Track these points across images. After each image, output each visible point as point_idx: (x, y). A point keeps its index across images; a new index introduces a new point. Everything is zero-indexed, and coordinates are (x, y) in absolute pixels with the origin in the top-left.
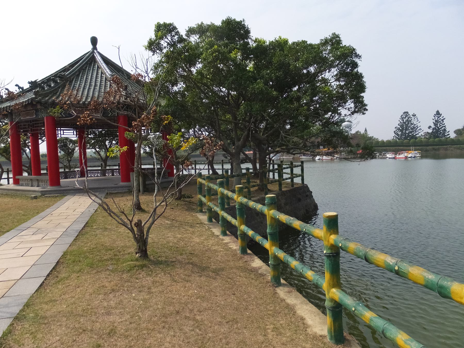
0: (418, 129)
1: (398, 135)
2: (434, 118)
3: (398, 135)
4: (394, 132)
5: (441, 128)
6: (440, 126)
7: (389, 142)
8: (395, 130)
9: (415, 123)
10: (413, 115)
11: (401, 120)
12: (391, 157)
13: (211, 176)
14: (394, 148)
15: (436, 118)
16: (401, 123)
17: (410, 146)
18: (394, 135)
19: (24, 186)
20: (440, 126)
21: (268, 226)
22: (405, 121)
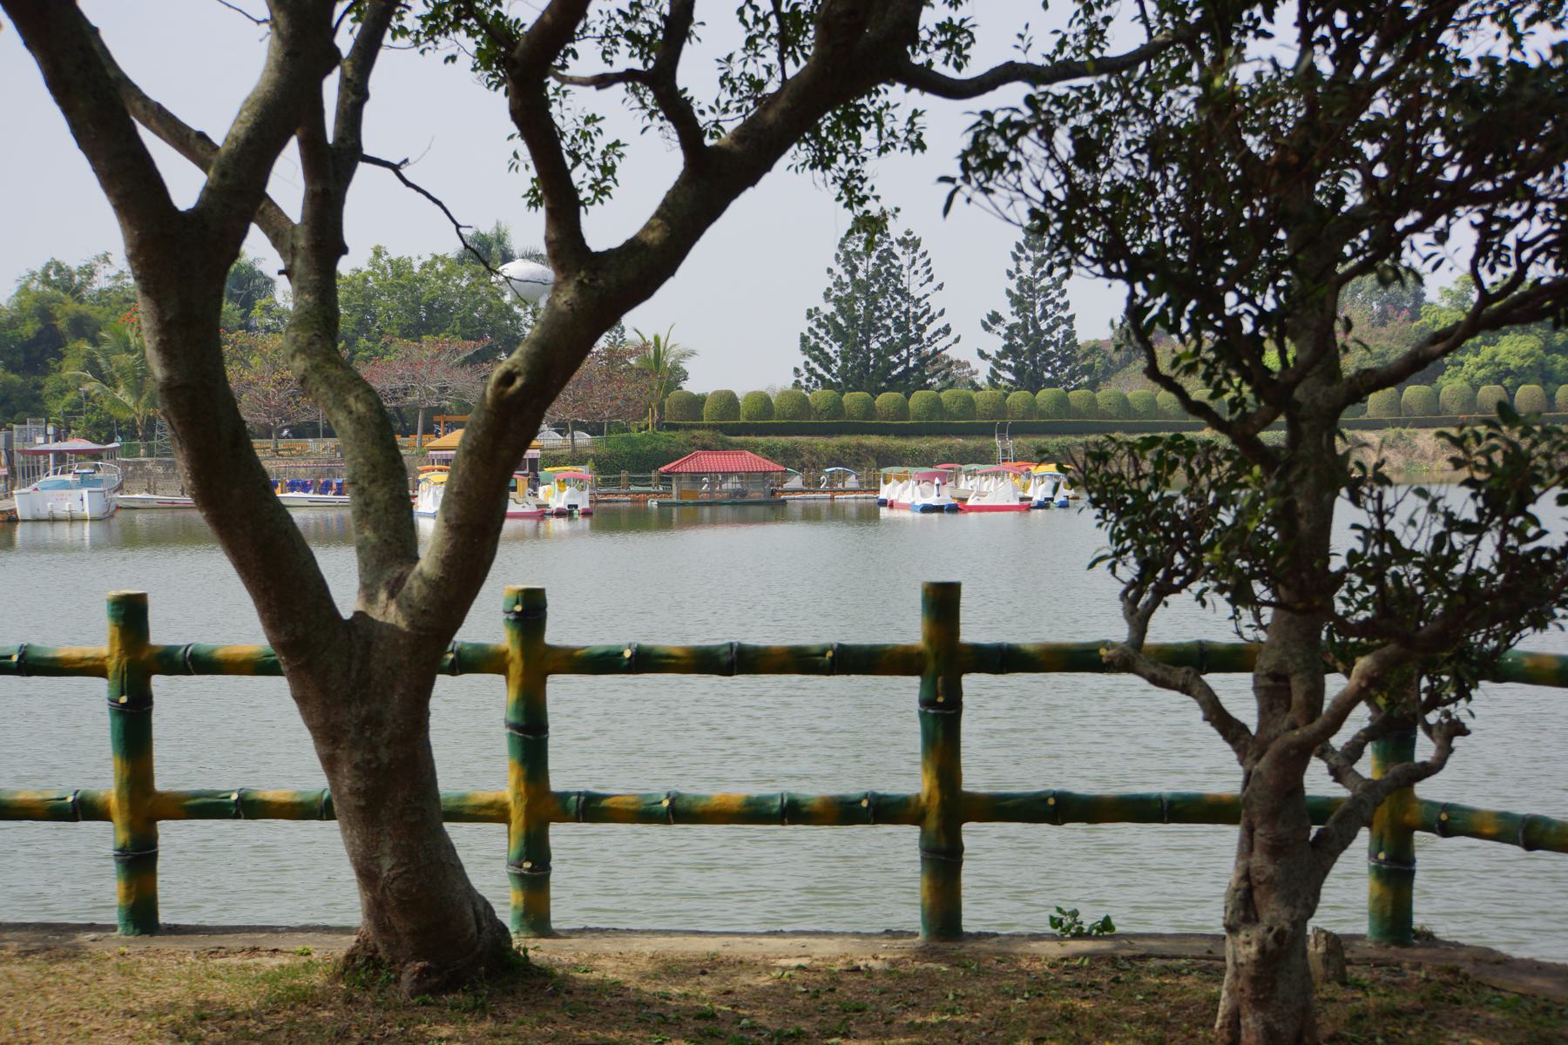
0: (931, 329)
1: (826, 361)
2: (1012, 266)
3: (826, 361)
4: (804, 339)
5: (1050, 329)
6: (1045, 315)
7: (763, 403)
8: (805, 325)
9: (916, 292)
10: (903, 243)
11: (839, 270)
12: (933, 500)
13: (957, 466)
14: (836, 441)
15: (1026, 268)
16: (839, 284)
17: (986, 431)
18: (800, 359)
19: (71, 452)
20: (1045, 315)
21: (1220, 1014)
22: (861, 275)
